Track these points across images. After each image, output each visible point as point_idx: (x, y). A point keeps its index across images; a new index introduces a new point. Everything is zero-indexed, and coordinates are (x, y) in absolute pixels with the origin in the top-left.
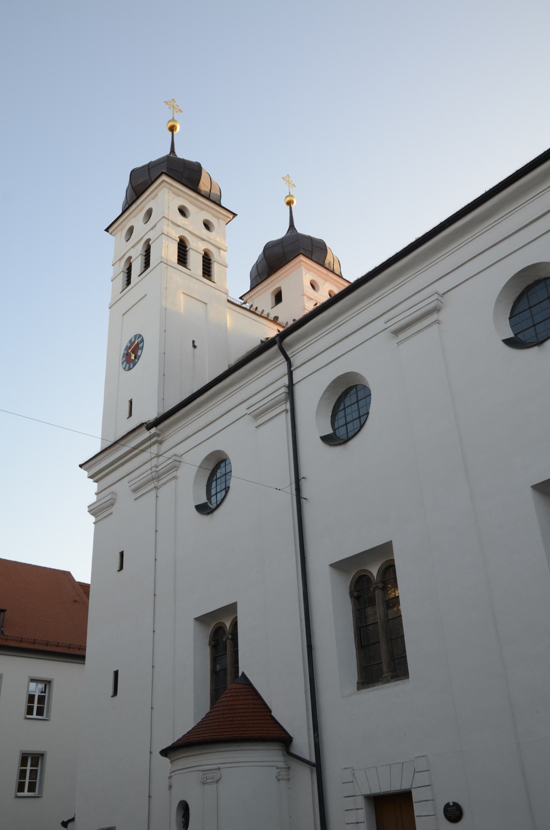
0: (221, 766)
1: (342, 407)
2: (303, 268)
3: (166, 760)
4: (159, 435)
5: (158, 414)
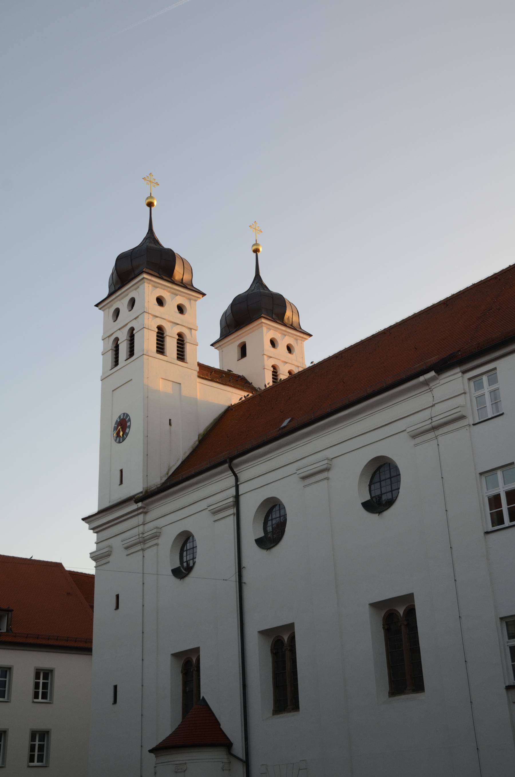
0: (187, 762)
1: (270, 518)
2: (265, 329)
3: (153, 755)
4: (144, 508)
5: (143, 488)
